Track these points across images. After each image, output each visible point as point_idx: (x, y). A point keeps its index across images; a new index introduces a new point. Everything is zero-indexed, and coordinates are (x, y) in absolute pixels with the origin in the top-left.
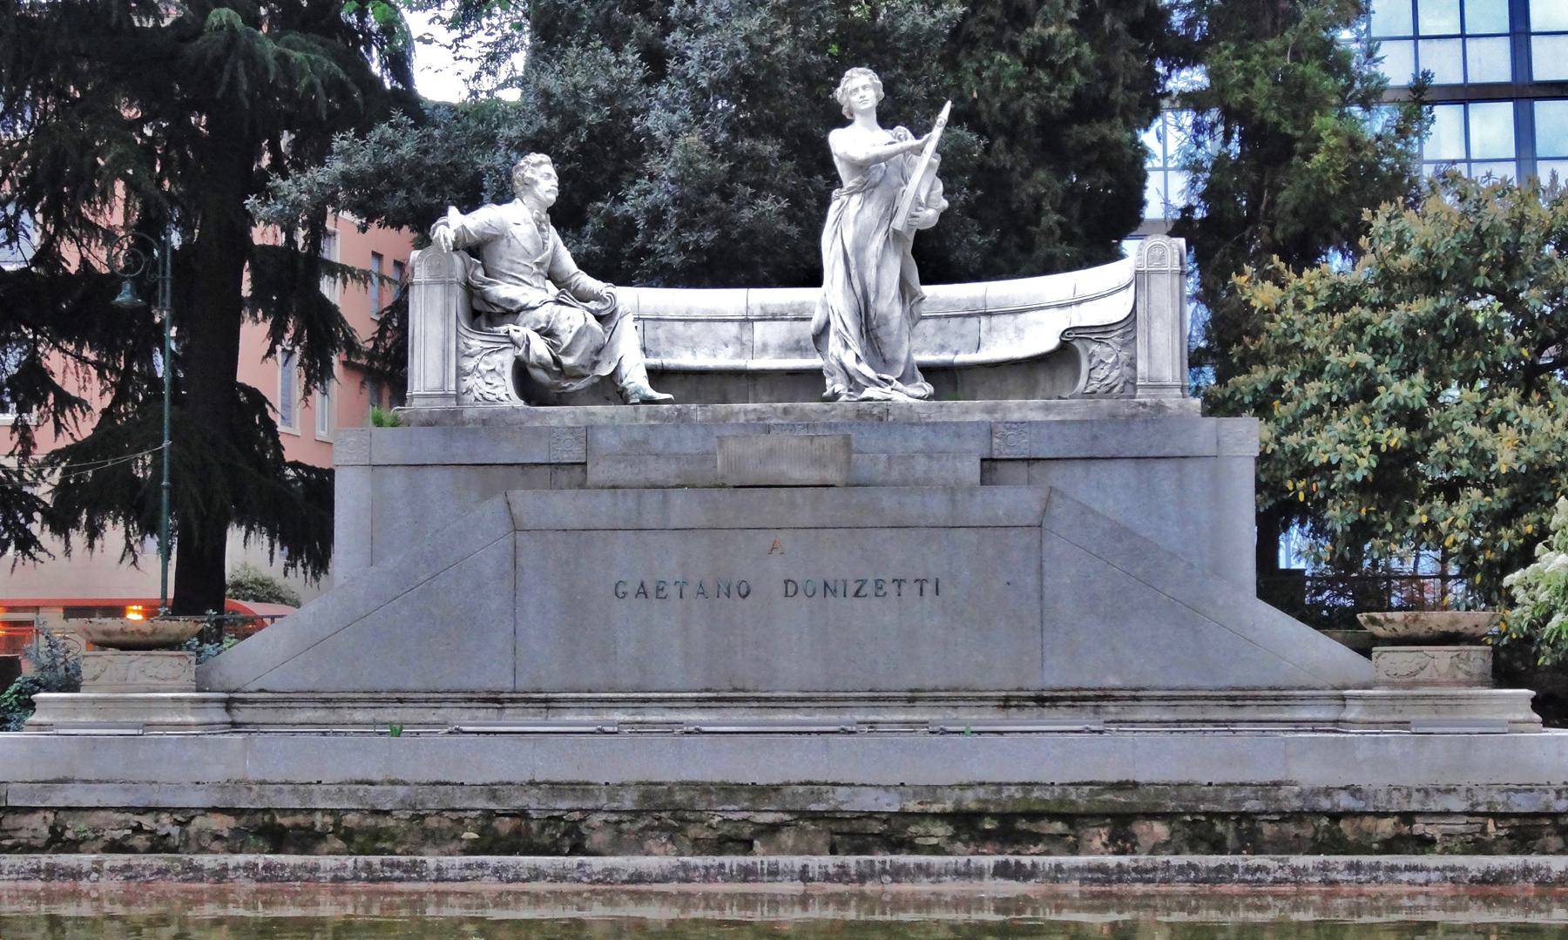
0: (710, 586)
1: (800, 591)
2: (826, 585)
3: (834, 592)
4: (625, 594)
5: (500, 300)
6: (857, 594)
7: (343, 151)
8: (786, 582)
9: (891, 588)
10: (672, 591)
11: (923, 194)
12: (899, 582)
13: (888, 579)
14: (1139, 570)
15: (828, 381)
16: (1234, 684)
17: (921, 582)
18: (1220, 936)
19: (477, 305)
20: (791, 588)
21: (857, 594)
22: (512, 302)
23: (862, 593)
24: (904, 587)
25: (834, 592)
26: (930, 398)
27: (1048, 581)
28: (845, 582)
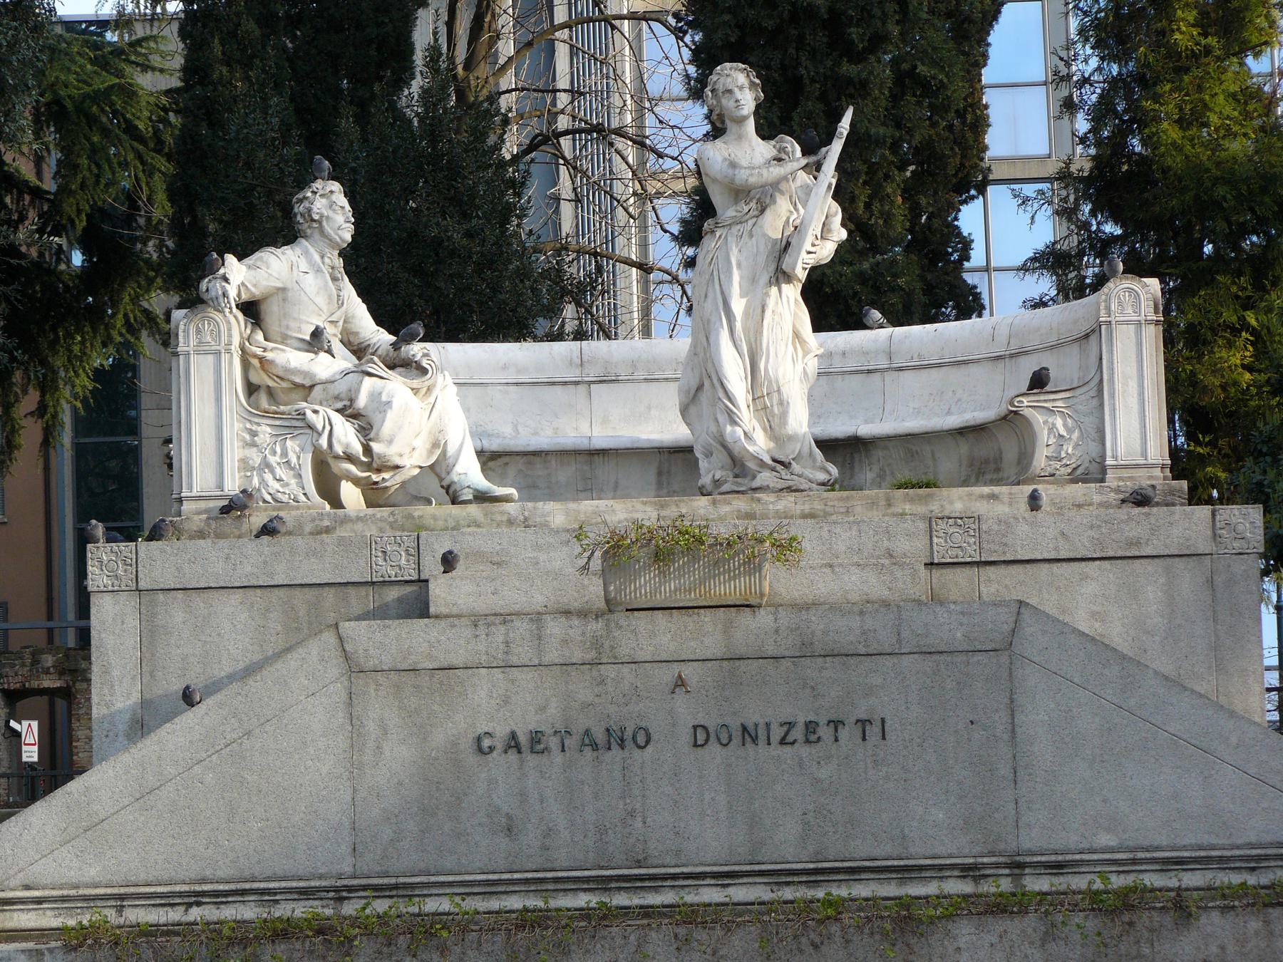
0: (600, 737)
1: (713, 739)
2: (744, 729)
3: (755, 740)
4: (491, 749)
5: (287, 370)
6: (783, 742)
7: (1076, 208)
8: (695, 727)
9: (825, 732)
10: (554, 743)
11: (821, 232)
12: (836, 724)
13: (823, 721)
14: (1132, 702)
15: (703, 464)
16: (1253, 839)
17: (863, 723)
18: (45, 455)
19: (255, 378)
20: (701, 736)
21: (783, 742)
22: (306, 374)
23: (790, 739)
24: (843, 733)
25: (755, 740)
26: (829, 485)
27: (1020, 718)
28: (768, 725)
